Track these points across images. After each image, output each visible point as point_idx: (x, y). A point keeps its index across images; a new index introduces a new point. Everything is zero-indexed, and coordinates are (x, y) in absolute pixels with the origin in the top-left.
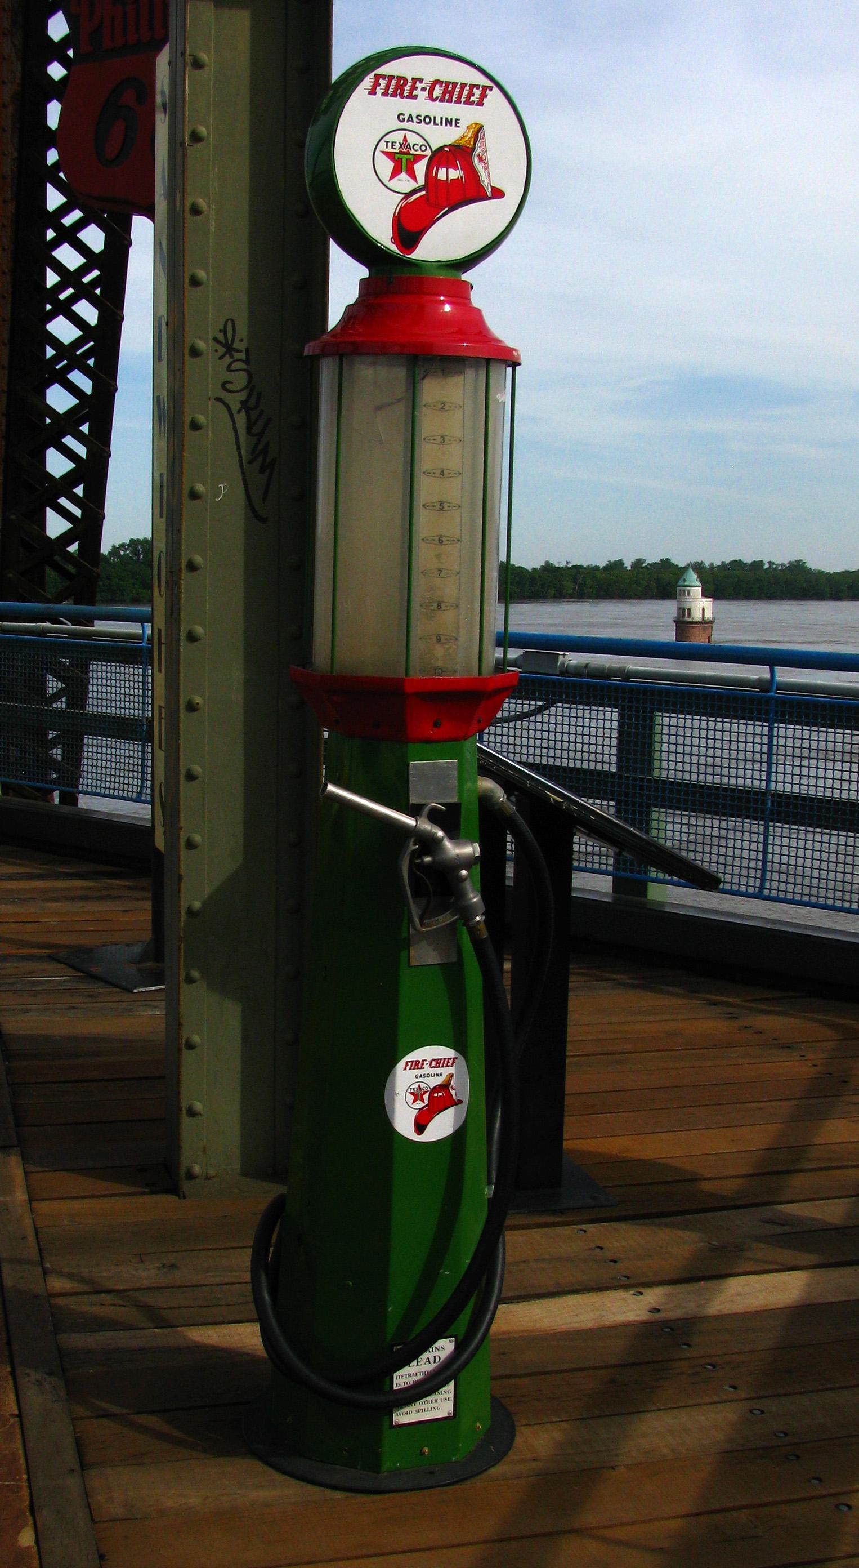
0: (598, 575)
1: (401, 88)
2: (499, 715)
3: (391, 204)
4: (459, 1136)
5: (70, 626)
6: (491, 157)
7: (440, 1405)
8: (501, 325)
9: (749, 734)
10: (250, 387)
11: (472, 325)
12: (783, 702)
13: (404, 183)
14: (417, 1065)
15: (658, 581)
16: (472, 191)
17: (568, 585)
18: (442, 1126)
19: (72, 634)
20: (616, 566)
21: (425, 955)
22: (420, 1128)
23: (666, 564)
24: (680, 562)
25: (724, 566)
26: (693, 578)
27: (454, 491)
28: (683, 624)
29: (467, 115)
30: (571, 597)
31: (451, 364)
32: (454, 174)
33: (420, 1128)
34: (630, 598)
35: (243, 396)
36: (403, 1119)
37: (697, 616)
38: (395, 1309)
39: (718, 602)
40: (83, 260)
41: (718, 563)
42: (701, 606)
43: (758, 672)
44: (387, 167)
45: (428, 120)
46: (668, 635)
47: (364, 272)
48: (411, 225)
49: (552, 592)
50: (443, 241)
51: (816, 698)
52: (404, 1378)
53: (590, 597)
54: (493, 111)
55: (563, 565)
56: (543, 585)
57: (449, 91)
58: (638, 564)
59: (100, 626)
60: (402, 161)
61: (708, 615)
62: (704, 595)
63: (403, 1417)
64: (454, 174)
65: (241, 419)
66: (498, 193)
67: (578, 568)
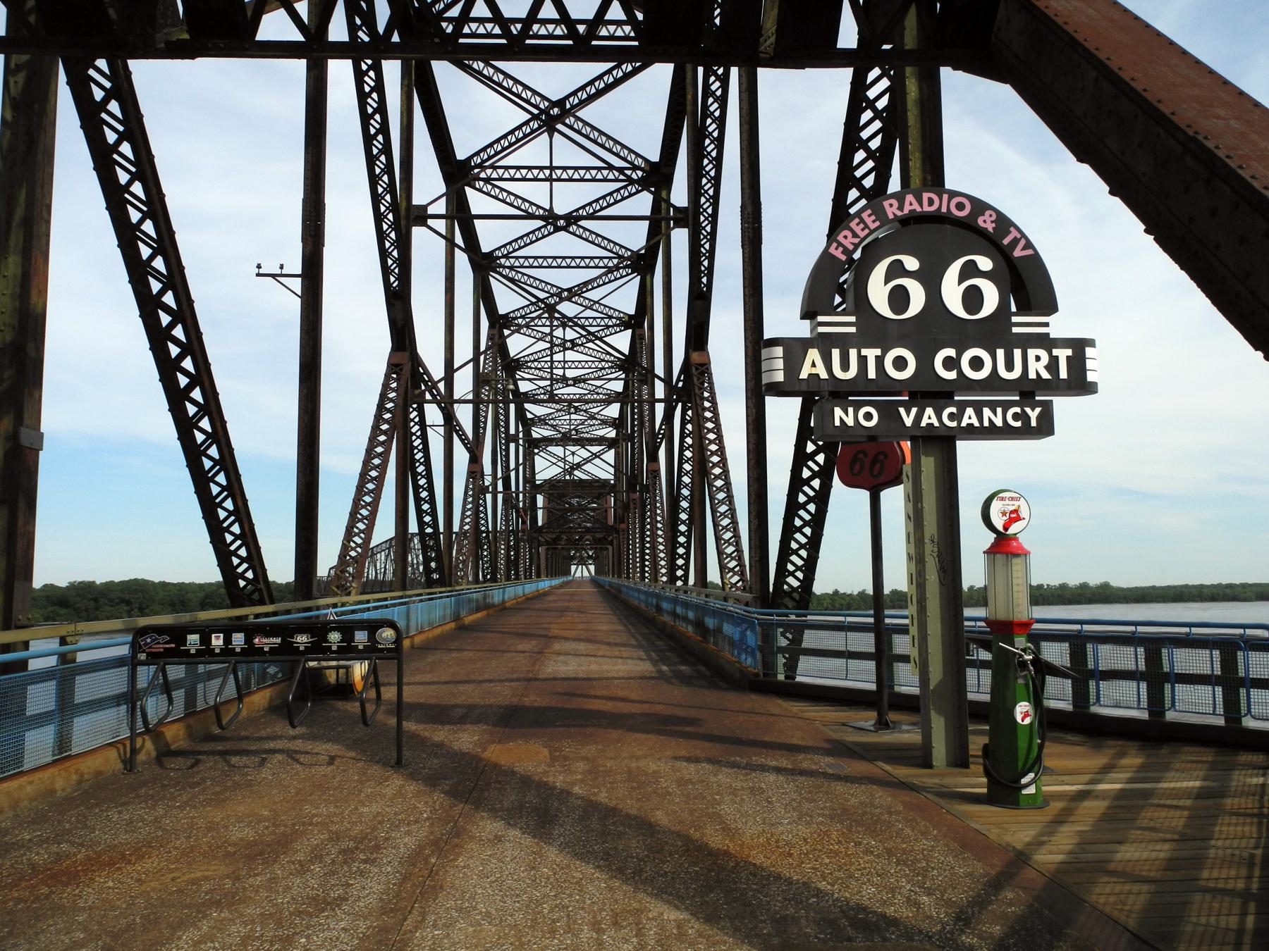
1: (1002, 499)
2: (937, 424)
4: (1031, 724)
8: (1027, 546)
11: (1020, 547)
16: (1018, 519)
18: (1028, 721)
21: (1021, 681)
27: (1020, 574)
29: (1017, 503)
31: (1018, 555)
38: (1020, 765)
43: (1239, 631)
48: (1006, 528)
50: (1011, 531)
52: (1024, 781)
54: (1022, 502)
57: (1012, 499)
59: (809, 617)
60: (1004, 514)
63: (1024, 792)
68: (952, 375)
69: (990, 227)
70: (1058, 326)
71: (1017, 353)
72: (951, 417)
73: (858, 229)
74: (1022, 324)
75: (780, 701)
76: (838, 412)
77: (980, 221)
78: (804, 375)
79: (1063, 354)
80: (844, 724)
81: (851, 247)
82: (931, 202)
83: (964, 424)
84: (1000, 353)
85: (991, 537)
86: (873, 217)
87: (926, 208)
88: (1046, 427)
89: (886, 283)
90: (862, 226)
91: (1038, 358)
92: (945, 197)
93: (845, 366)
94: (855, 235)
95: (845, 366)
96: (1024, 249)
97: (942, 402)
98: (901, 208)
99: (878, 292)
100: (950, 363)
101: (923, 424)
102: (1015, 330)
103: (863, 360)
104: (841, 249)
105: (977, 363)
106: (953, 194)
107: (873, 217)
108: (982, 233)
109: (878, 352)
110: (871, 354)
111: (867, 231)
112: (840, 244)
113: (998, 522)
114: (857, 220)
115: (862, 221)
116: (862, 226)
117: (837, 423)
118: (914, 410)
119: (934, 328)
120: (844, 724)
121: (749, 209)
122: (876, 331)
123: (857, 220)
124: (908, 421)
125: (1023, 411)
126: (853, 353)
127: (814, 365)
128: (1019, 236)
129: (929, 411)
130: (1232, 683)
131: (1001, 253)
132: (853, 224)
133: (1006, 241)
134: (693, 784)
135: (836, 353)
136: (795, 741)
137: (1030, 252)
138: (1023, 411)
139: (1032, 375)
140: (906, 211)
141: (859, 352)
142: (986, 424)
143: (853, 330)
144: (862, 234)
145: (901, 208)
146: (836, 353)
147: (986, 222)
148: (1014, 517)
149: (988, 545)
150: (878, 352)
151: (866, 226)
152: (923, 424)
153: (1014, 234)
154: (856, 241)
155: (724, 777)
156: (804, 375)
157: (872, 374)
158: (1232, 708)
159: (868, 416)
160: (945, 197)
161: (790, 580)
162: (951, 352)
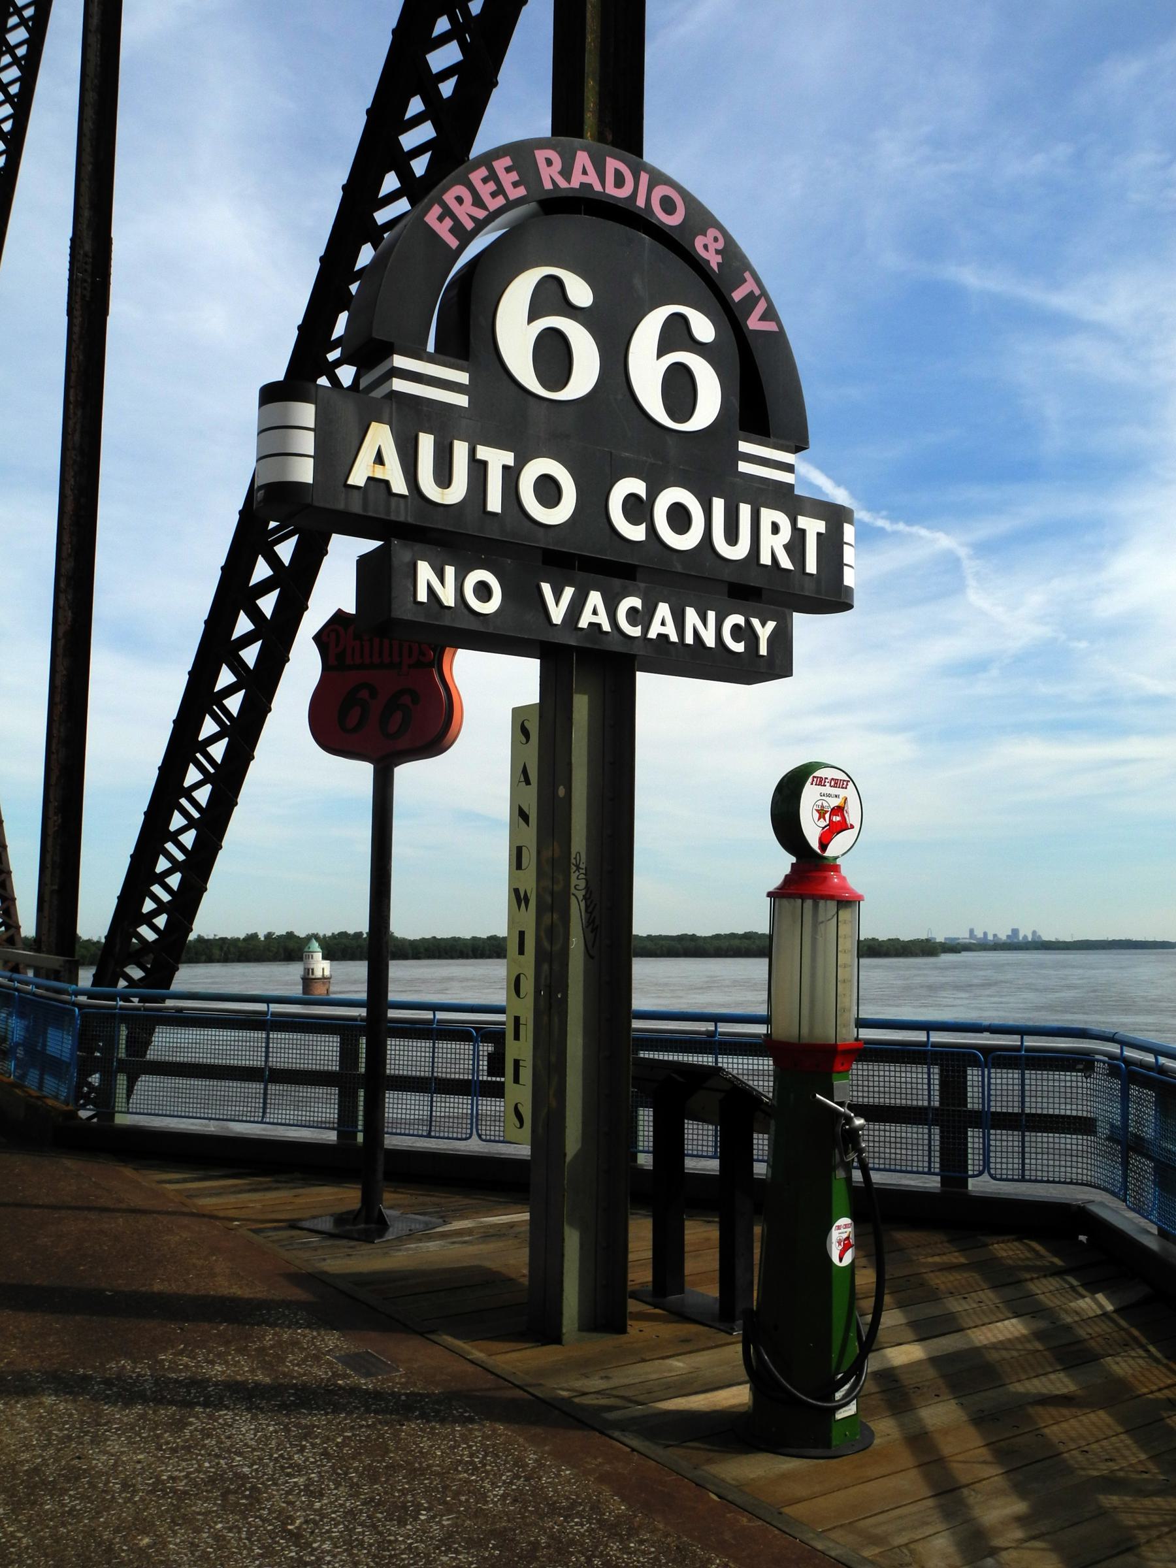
0: (240, 944)
1: (821, 782)
2: (606, 627)
3: (819, 831)
5: (121, 1003)
6: (850, 811)
7: (851, 1409)
9: (279, 1061)
10: (587, 888)
12: (721, 1043)
13: (823, 823)
14: (839, 1228)
15: (287, 949)
16: (843, 826)
17: (216, 952)
19: (121, 1008)
20: (253, 937)
22: (841, 1260)
23: (290, 935)
24: (301, 933)
25: (334, 936)
26: (315, 945)
28: (308, 981)
30: (218, 961)
32: (838, 818)
33: (841, 1260)
34: (264, 961)
35: (583, 892)
36: (835, 1258)
37: (318, 974)
39: (335, 963)
40: (201, 777)
41: (329, 934)
42: (321, 966)
43: (710, 1027)
44: (816, 815)
45: (829, 795)
46: (297, 991)
47: (793, 860)
49: (204, 958)
51: (744, 1040)
52: (838, 1395)
53: (233, 961)
55: (211, 937)
56: (196, 953)
57: (836, 783)
58: (269, 936)
60: (821, 813)
61: (327, 973)
62: (324, 958)
63: (840, 1415)
64: (838, 818)
65: (583, 904)
66: (852, 827)
67: (223, 940)
68: (637, 533)
69: (714, 260)
70: (809, 474)
71: (745, 510)
72: (632, 613)
73: (485, 190)
74: (756, 458)
75: (128, 1172)
76: (425, 572)
77: (699, 243)
78: (358, 478)
79: (813, 527)
80: (293, 1225)
81: (469, 225)
82: (619, 181)
83: (652, 634)
84: (718, 504)
85: (783, 863)
86: (514, 176)
87: (611, 190)
88: (774, 664)
89: (531, 319)
90: (492, 186)
91: (775, 529)
92: (644, 178)
93: (444, 477)
94: (478, 202)
95: (444, 477)
96: (763, 318)
97: (617, 583)
98: (566, 173)
99: (515, 335)
100: (637, 509)
101: (583, 623)
102: (744, 467)
103: (478, 469)
104: (448, 223)
105: (679, 518)
106: (658, 178)
107: (514, 176)
108: (698, 266)
109: (508, 458)
110: (497, 459)
111: (500, 201)
112: (447, 212)
113: (812, 830)
114: (483, 172)
115: (492, 176)
116: (492, 186)
117: (422, 596)
118: (569, 592)
119: (605, 435)
120: (293, 1225)
121: (87, 247)
122: (504, 413)
123: (483, 172)
124: (557, 614)
125: (748, 622)
126: (461, 450)
127: (379, 459)
128: (757, 292)
129: (595, 598)
130: (952, 1119)
131: (731, 317)
132: (476, 177)
133: (737, 295)
134: (56, 1491)
135: (426, 443)
136: (226, 1287)
137: (770, 326)
138: (748, 622)
139: (765, 559)
140: (575, 183)
141: (472, 452)
142: (689, 639)
143: (462, 400)
144: (494, 204)
145: (566, 173)
146: (426, 443)
147: (707, 248)
148: (837, 822)
149: (776, 881)
150: (508, 458)
151: (500, 191)
152: (583, 623)
153: (748, 287)
154: (481, 214)
155: (123, 1448)
156: (358, 478)
157: (494, 504)
158: (953, 1162)
159: (483, 591)
160: (644, 178)
161: (145, 932)
162: (637, 486)
